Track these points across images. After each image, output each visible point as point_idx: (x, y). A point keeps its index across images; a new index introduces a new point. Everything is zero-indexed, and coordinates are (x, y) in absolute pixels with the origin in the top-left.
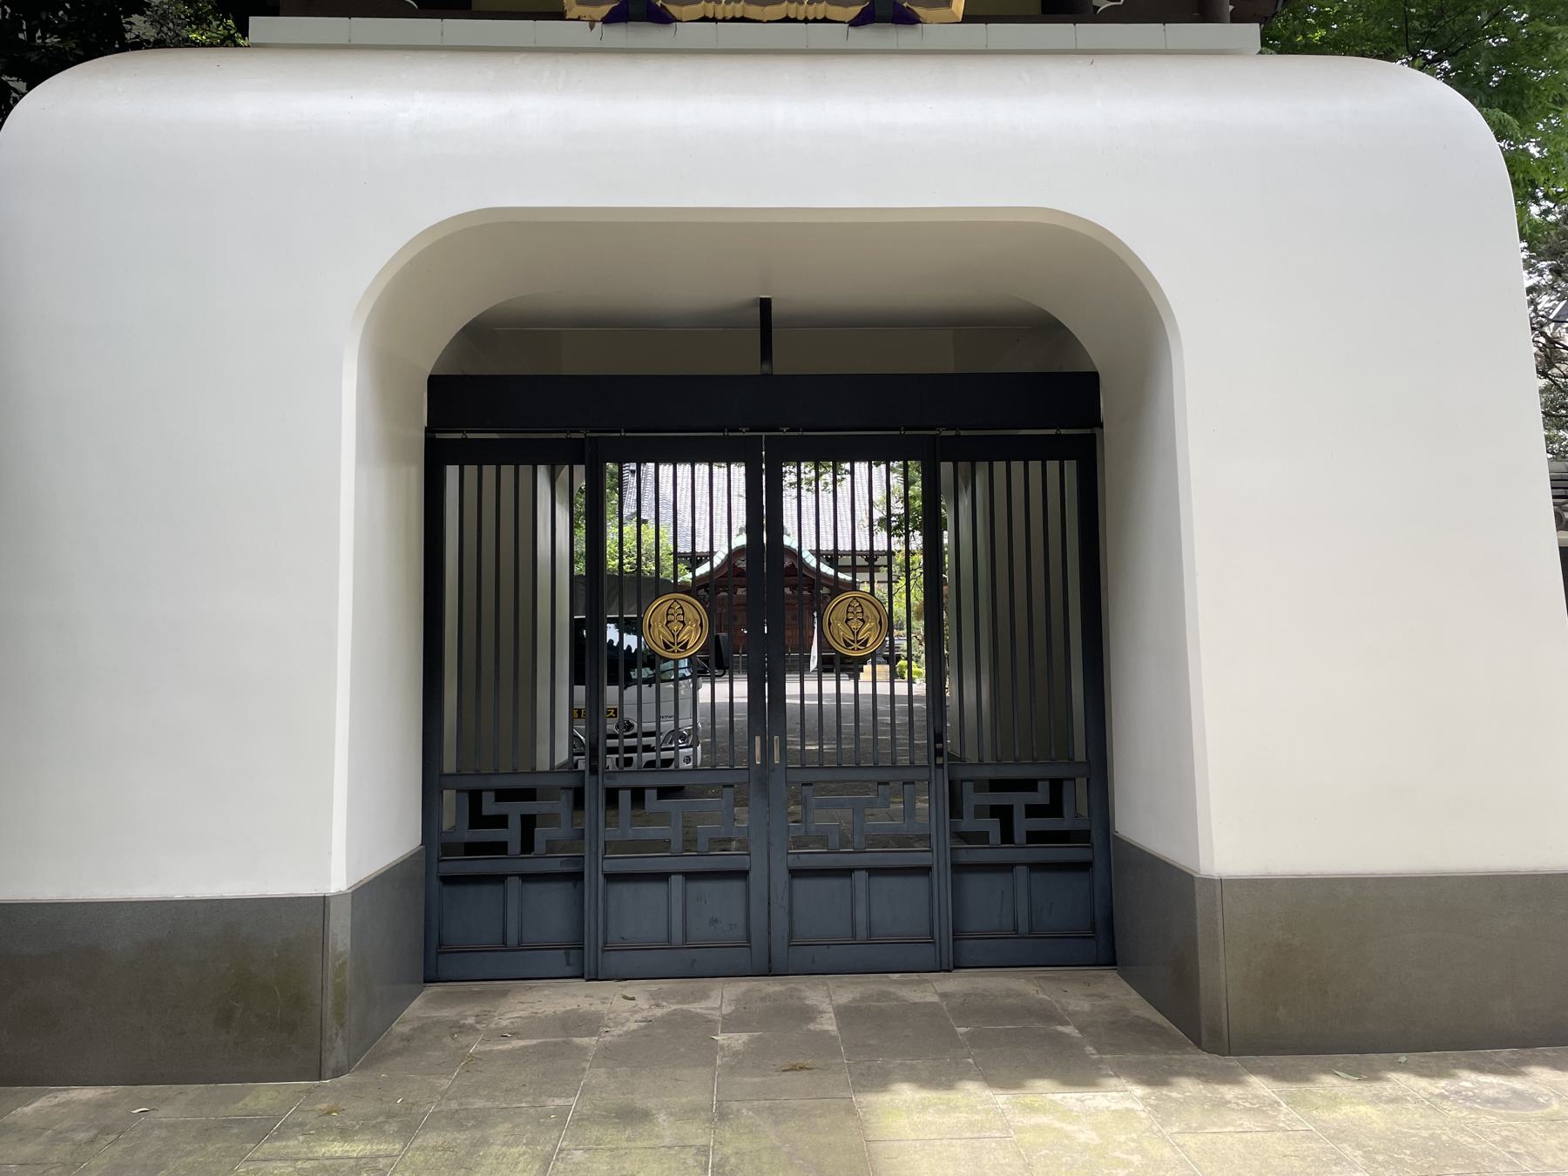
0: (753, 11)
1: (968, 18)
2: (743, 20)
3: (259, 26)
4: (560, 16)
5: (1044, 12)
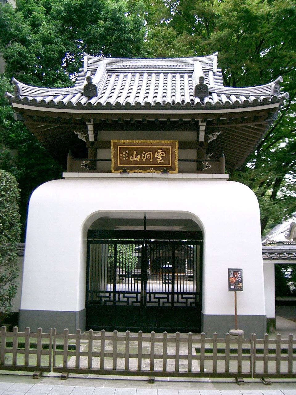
0: (142, 171)
1: (179, 172)
2: (141, 173)
3: (64, 174)
4: (110, 172)
5: (197, 170)
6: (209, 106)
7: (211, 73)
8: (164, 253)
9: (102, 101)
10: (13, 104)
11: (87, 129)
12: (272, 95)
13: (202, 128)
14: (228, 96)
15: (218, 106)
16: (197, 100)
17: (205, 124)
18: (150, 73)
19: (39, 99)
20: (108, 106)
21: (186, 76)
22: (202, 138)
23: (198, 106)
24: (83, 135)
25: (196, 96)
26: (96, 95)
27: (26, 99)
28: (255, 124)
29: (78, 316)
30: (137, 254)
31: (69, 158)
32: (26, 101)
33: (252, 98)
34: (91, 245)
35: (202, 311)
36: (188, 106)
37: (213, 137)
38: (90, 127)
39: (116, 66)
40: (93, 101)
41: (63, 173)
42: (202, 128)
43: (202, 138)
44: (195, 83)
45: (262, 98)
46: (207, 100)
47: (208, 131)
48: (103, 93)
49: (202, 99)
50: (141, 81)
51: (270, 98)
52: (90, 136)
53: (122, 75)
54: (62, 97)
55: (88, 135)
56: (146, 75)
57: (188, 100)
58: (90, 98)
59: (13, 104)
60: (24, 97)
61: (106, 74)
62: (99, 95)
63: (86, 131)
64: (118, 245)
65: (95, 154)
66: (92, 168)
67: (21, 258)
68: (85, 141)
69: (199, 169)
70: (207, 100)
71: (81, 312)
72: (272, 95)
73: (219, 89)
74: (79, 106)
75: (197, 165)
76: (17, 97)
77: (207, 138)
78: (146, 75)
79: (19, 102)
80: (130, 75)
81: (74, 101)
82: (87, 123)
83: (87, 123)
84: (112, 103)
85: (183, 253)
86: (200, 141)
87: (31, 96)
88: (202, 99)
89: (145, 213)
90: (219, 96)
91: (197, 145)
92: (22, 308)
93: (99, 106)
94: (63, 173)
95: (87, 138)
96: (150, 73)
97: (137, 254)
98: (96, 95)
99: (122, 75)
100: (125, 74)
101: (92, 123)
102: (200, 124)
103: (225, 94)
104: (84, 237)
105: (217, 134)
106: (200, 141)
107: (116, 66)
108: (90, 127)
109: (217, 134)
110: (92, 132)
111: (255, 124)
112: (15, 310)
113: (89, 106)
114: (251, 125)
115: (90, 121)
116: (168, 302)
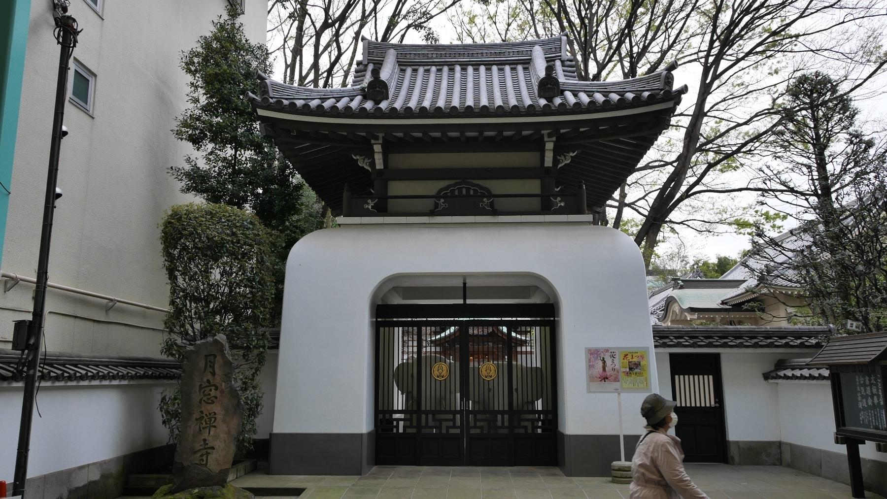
6: (564, 109)
7: (558, 63)
8: (476, 347)
9: (398, 105)
10: (258, 110)
11: (373, 152)
12: (661, 90)
13: (550, 146)
14: (590, 94)
15: (578, 108)
16: (543, 102)
17: (554, 139)
18: (464, 67)
19: (300, 103)
20: (408, 112)
21: (520, 68)
22: (549, 161)
23: (547, 111)
24: (366, 160)
25: (540, 96)
26: (387, 98)
27: (279, 102)
28: (632, 135)
29: (365, 440)
30: (433, 349)
31: (345, 195)
32: (278, 106)
33: (630, 96)
34: (382, 329)
35: (561, 429)
36: (532, 110)
37: (566, 160)
38: (377, 148)
39: (412, 56)
40: (383, 105)
41: (860, 446)
42: (550, 146)
43: (549, 161)
44: (535, 77)
45: (646, 94)
46: (558, 101)
47: (558, 151)
48: (396, 97)
49: (550, 100)
50: (451, 77)
51: (658, 94)
52: (377, 161)
53: (421, 70)
54: (333, 100)
55: (374, 160)
56: (458, 68)
57: (528, 102)
58: (377, 102)
59: (258, 110)
60: (275, 100)
61: (397, 70)
62: (390, 96)
63: (370, 154)
64: (424, 328)
65: (386, 188)
66: (382, 210)
67: (273, 351)
68: (369, 169)
69: (546, 208)
70: (558, 101)
71: (369, 434)
72: (661, 90)
73: (575, 85)
74: (362, 113)
75: (542, 203)
76: (265, 100)
77: (556, 161)
78: (458, 68)
79: (269, 107)
80: (434, 69)
81: (354, 104)
82: (373, 141)
83: (373, 141)
84: (413, 108)
85: (500, 346)
86: (546, 165)
87: (286, 99)
88: (550, 100)
89: (465, 276)
90: (575, 95)
91: (538, 172)
92: (277, 430)
93: (393, 113)
94: (860, 446)
95: (373, 164)
96: (464, 67)
97: (433, 349)
98: (387, 98)
99: (421, 70)
100: (426, 68)
101: (381, 141)
102: (546, 139)
103: (585, 92)
104: (372, 317)
105: (571, 154)
106: (546, 165)
107: (412, 56)
108: (377, 148)
109: (571, 154)
110: (381, 156)
111: (632, 135)
112: (261, 435)
113: (378, 113)
114: (629, 138)
115: (377, 138)
116: (454, 427)
